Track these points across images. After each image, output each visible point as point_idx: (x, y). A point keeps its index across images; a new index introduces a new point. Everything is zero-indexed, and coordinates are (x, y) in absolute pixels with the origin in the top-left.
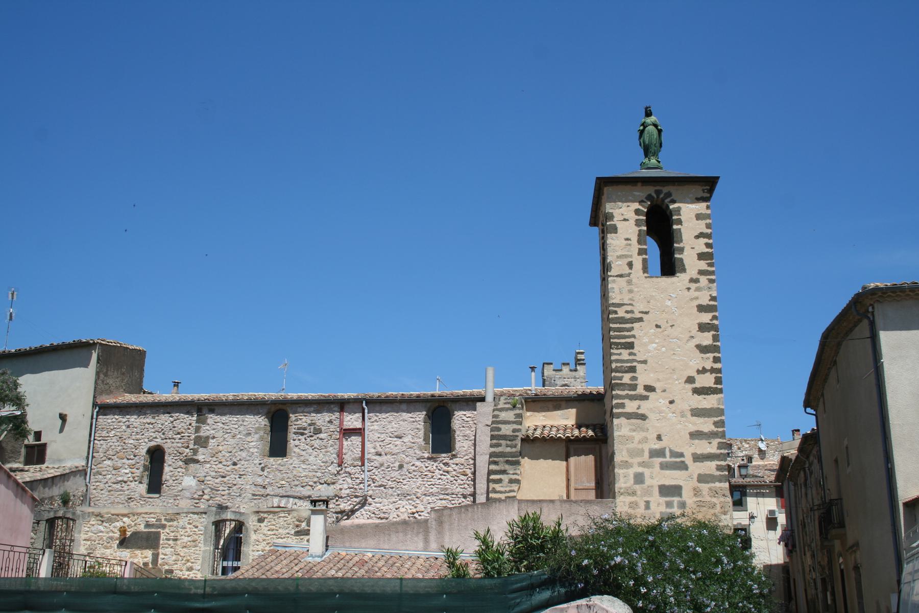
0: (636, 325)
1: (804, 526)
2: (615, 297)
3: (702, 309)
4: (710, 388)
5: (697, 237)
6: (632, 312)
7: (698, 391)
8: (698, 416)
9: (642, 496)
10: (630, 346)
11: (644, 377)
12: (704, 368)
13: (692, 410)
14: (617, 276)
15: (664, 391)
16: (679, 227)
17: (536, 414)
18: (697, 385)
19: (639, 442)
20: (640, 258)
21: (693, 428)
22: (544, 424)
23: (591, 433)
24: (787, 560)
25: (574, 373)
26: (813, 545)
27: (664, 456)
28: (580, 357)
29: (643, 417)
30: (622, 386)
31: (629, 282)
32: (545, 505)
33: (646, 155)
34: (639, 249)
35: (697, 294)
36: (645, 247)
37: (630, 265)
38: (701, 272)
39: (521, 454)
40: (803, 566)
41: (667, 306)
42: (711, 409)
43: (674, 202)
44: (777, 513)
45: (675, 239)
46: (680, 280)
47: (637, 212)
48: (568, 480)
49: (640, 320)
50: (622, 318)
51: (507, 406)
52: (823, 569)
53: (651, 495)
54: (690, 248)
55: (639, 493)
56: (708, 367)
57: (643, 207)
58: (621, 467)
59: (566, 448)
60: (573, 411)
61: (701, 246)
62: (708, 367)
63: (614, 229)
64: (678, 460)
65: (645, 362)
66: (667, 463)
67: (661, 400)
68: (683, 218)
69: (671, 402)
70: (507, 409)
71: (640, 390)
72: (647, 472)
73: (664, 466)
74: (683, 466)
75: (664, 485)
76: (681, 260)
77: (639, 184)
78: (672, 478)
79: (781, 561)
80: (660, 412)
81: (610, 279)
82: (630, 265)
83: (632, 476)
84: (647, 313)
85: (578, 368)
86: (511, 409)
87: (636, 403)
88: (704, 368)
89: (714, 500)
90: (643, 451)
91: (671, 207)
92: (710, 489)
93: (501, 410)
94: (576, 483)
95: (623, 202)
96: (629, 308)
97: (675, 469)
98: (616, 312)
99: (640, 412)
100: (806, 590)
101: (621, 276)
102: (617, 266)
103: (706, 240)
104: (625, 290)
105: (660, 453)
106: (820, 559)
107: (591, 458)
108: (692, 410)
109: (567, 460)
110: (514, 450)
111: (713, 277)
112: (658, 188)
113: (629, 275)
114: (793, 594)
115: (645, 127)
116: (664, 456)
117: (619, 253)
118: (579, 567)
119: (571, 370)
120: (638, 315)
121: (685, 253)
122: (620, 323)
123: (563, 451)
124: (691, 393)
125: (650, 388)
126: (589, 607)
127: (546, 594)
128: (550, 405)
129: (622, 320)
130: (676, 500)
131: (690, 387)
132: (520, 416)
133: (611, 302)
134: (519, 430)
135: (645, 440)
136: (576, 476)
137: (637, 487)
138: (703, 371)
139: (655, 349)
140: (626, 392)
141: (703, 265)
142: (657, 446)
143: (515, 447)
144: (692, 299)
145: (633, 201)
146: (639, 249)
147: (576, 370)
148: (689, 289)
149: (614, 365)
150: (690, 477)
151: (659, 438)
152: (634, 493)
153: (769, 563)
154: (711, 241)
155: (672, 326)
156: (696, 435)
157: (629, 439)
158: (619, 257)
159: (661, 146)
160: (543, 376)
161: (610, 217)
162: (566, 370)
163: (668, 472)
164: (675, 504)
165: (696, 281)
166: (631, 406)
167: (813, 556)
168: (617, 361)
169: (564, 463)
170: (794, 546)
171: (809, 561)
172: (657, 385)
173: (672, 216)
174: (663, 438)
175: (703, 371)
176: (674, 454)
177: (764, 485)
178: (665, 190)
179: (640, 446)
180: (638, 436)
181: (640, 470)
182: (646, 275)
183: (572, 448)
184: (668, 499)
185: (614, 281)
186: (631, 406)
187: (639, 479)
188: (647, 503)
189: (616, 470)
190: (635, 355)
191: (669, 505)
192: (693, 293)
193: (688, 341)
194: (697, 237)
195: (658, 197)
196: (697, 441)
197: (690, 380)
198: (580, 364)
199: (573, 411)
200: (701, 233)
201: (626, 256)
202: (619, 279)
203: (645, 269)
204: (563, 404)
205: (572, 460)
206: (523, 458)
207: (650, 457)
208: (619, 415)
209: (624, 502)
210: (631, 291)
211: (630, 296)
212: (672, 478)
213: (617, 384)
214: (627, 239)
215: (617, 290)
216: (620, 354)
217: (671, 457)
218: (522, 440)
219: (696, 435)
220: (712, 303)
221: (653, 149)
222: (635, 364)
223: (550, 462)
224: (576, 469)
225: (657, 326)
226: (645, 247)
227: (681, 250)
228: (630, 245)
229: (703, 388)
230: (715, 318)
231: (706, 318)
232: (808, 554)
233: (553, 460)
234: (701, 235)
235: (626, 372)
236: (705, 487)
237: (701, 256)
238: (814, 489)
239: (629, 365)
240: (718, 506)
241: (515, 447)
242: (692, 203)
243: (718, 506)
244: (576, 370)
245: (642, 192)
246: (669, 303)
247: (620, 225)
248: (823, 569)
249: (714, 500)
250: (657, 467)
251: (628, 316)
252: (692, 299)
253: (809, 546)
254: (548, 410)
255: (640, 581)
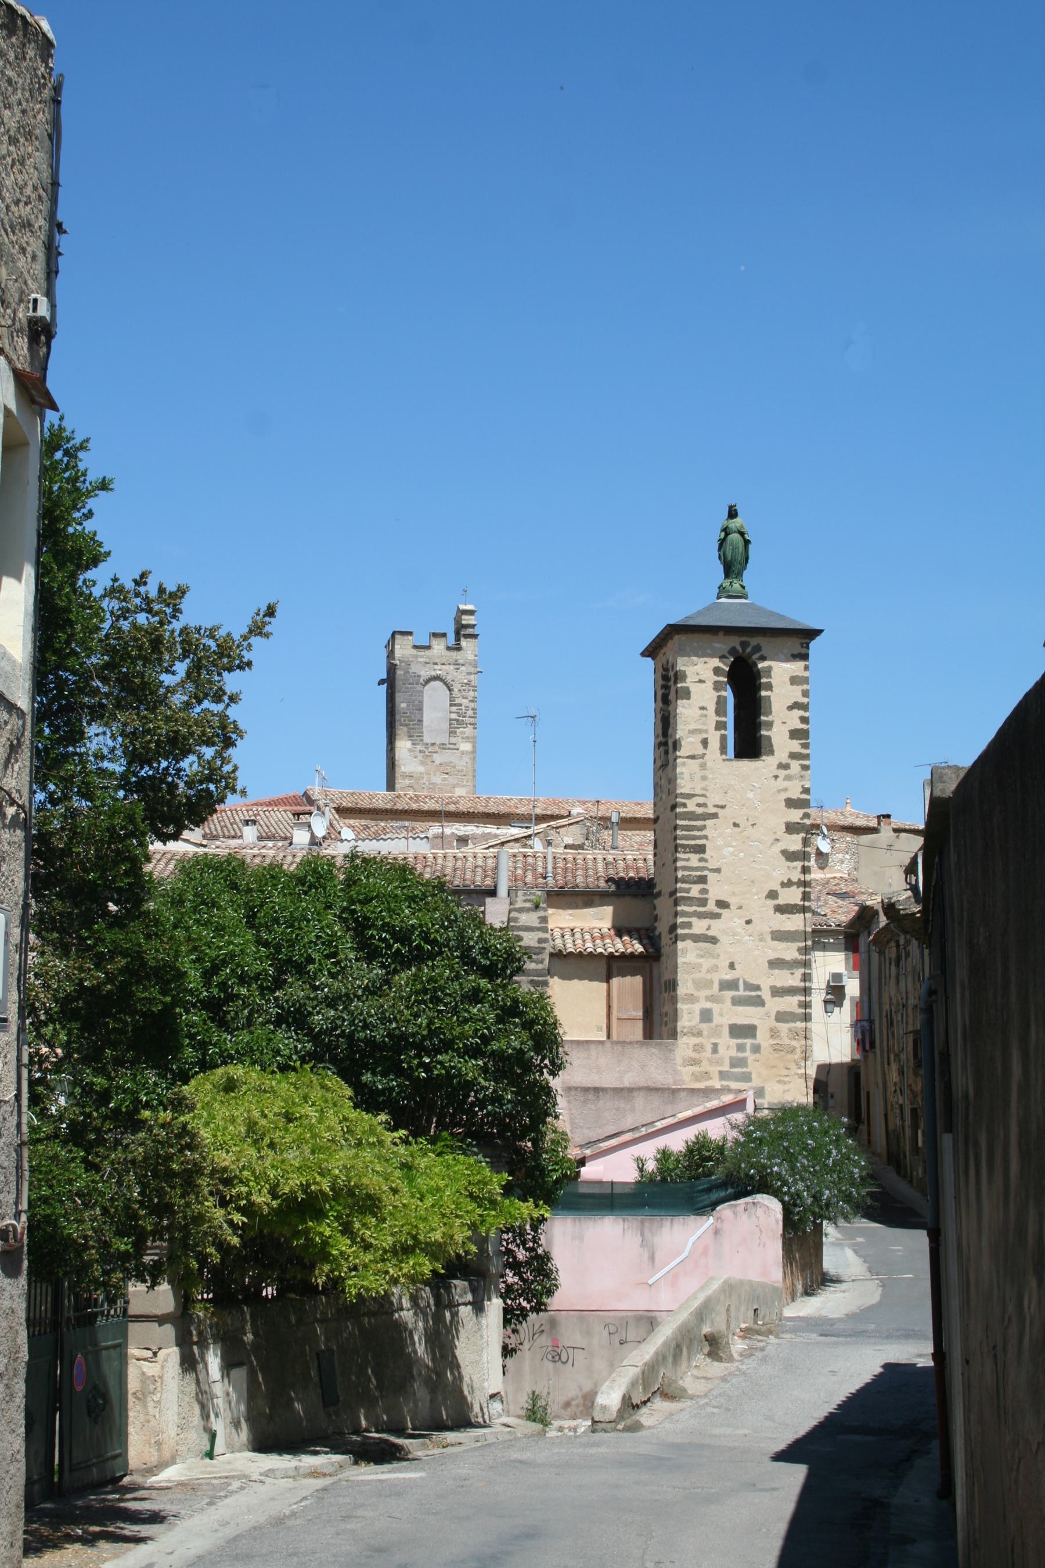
0: (709, 823)
1: (891, 1023)
2: (684, 785)
3: (791, 803)
4: (796, 905)
5: (790, 708)
6: (704, 805)
7: (781, 909)
8: (780, 940)
9: (709, 1037)
10: (701, 849)
11: (716, 890)
12: (789, 880)
13: (772, 933)
14: (688, 757)
15: (740, 908)
16: (768, 693)
17: (560, 911)
18: (781, 901)
19: (708, 971)
20: (718, 733)
21: (772, 955)
22: (572, 925)
23: (639, 948)
24: (858, 1057)
25: (454, 654)
26: (903, 1057)
27: (737, 989)
28: (466, 620)
29: (714, 940)
30: (689, 900)
31: (703, 766)
32: (593, 1047)
33: (727, 575)
34: (717, 722)
35: (787, 784)
36: (723, 719)
37: (705, 743)
38: (793, 756)
39: (550, 972)
40: (885, 1084)
41: (748, 799)
42: (796, 931)
43: (763, 658)
44: (845, 978)
45: (762, 710)
46: (766, 765)
47: (717, 671)
48: (609, 1007)
49: (715, 816)
50: (693, 813)
51: (528, 905)
52: (915, 1096)
53: (719, 1036)
54: (779, 725)
55: (705, 1033)
56: (795, 880)
57: (725, 664)
58: (684, 1001)
59: (611, 966)
60: (608, 910)
61: (794, 719)
62: (795, 880)
63: (686, 694)
64: (753, 993)
65: (718, 870)
66: (740, 997)
67: (736, 920)
68: (774, 681)
69: (748, 922)
70: (528, 910)
71: (711, 906)
72: (716, 1008)
73: (737, 1002)
74: (759, 1002)
75: (735, 1025)
76: (769, 738)
77: (721, 634)
78: (745, 1015)
79: (846, 1058)
80: (734, 935)
81: (679, 761)
82: (705, 743)
83: (698, 1013)
84: (723, 807)
85: (464, 643)
86: (533, 910)
87: (706, 922)
88: (789, 880)
89: (794, 1043)
90: (711, 982)
91: (760, 665)
92: (790, 1030)
93: (521, 910)
94: (618, 1011)
95: (699, 656)
96: (701, 800)
97: (749, 1005)
98: (684, 805)
99: (710, 933)
100: (886, 1116)
101: (693, 757)
102: (689, 744)
103: (801, 713)
104: (697, 777)
105: (732, 985)
106: (911, 1081)
107: (638, 980)
108: (772, 933)
109: (608, 982)
110: (540, 966)
111: (806, 762)
112: (744, 639)
113: (703, 756)
114: (864, 1115)
115: (727, 535)
116: (737, 989)
117: (692, 727)
118: (747, 1175)
119: (449, 648)
120: (712, 810)
121: (774, 729)
122: (690, 820)
123: (603, 969)
124: (772, 911)
125: (722, 904)
126: (754, 1203)
127: (722, 1194)
128: (579, 900)
129: (693, 816)
130: (748, 1042)
131: (772, 903)
132: (544, 920)
133: (679, 791)
134: (545, 941)
135: (715, 968)
136: (619, 1002)
137: (704, 1026)
138: (788, 884)
139: (732, 854)
140: (694, 908)
141: (795, 746)
142: (729, 976)
143: (542, 962)
144: (779, 791)
145: (712, 656)
146: (717, 722)
147: (458, 648)
148: (776, 777)
149: (680, 874)
150: (767, 1015)
151: (732, 966)
152: (699, 1034)
153: (827, 1061)
154: (806, 714)
155: (753, 825)
156: (776, 964)
157: (697, 967)
158: (692, 732)
159: (747, 562)
160: (391, 655)
161: (679, 676)
162: (439, 647)
163: (741, 1008)
164: (748, 1048)
165: (785, 767)
166: (699, 926)
167: (901, 1072)
168: (684, 868)
169: (605, 985)
170: (872, 1045)
171: (894, 1076)
172: (732, 901)
173: (760, 678)
174: (736, 966)
175: (788, 884)
176: (749, 987)
177: (825, 931)
178: (754, 641)
179: (709, 977)
180: (706, 963)
181: (708, 1005)
182: (724, 757)
183: (615, 966)
184: (739, 1041)
185: (684, 764)
186: (699, 926)
187: (706, 1016)
188: (715, 1046)
189: (679, 1006)
190: (706, 861)
191: (741, 1048)
192: (781, 783)
193: (772, 844)
194: (790, 708)
195: (744, 650)
196: (777, 971)
197: (772, 895)
198: (467, 636)
199: (608, 910)
200: (796, 703)
201: (700, 731)
202: (690, 761)
203: (723, 750)
204: (597, 899)
205: (615, 981)
206: (552, 977)
207: (721, 990)
208: (685, 937)
209: (688, 1044)
210: (704, 778)
211: (704, 784)
212: (745, 1015)
213: (683, 898)
214: (703, 708)
215: (687, 776)
216: (688, 860)
217: (745, 990)
218: (551, 955)
219: (776, 964)
220: (804, 796)
221: (737, 567)
222: (706, 873)
223: (586, 983)
224: (619, 994)
225: (736, 825)
226: (723, 719)
227: (770, 725)
228: (706, 716)
229: (787, 905)
230: (806, 816)
231: (795, 815)
232: (894, 1067)
233: (591, 980)
234: (796, 706)
235: (695, 883)
236: (784, 1027)
237: (795, 734)
238: (910, 979)
239: (698, 873)
240: (798, 1051)
241: (542, 962)
242: (786, 661)
243: (798, 1051)
244: (458, 648)
245: (724, 644)
246: (751, 795)
247: (694, 688)
248: (915, 1096)
249: (794, 1043)
250: (729, 1002)
251: (700, 811)
252: (779, 791)
253: (897, 1056)
254: (577, 907)
255: (785, 1183)
